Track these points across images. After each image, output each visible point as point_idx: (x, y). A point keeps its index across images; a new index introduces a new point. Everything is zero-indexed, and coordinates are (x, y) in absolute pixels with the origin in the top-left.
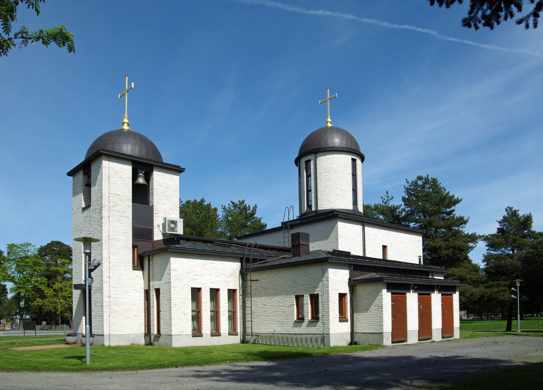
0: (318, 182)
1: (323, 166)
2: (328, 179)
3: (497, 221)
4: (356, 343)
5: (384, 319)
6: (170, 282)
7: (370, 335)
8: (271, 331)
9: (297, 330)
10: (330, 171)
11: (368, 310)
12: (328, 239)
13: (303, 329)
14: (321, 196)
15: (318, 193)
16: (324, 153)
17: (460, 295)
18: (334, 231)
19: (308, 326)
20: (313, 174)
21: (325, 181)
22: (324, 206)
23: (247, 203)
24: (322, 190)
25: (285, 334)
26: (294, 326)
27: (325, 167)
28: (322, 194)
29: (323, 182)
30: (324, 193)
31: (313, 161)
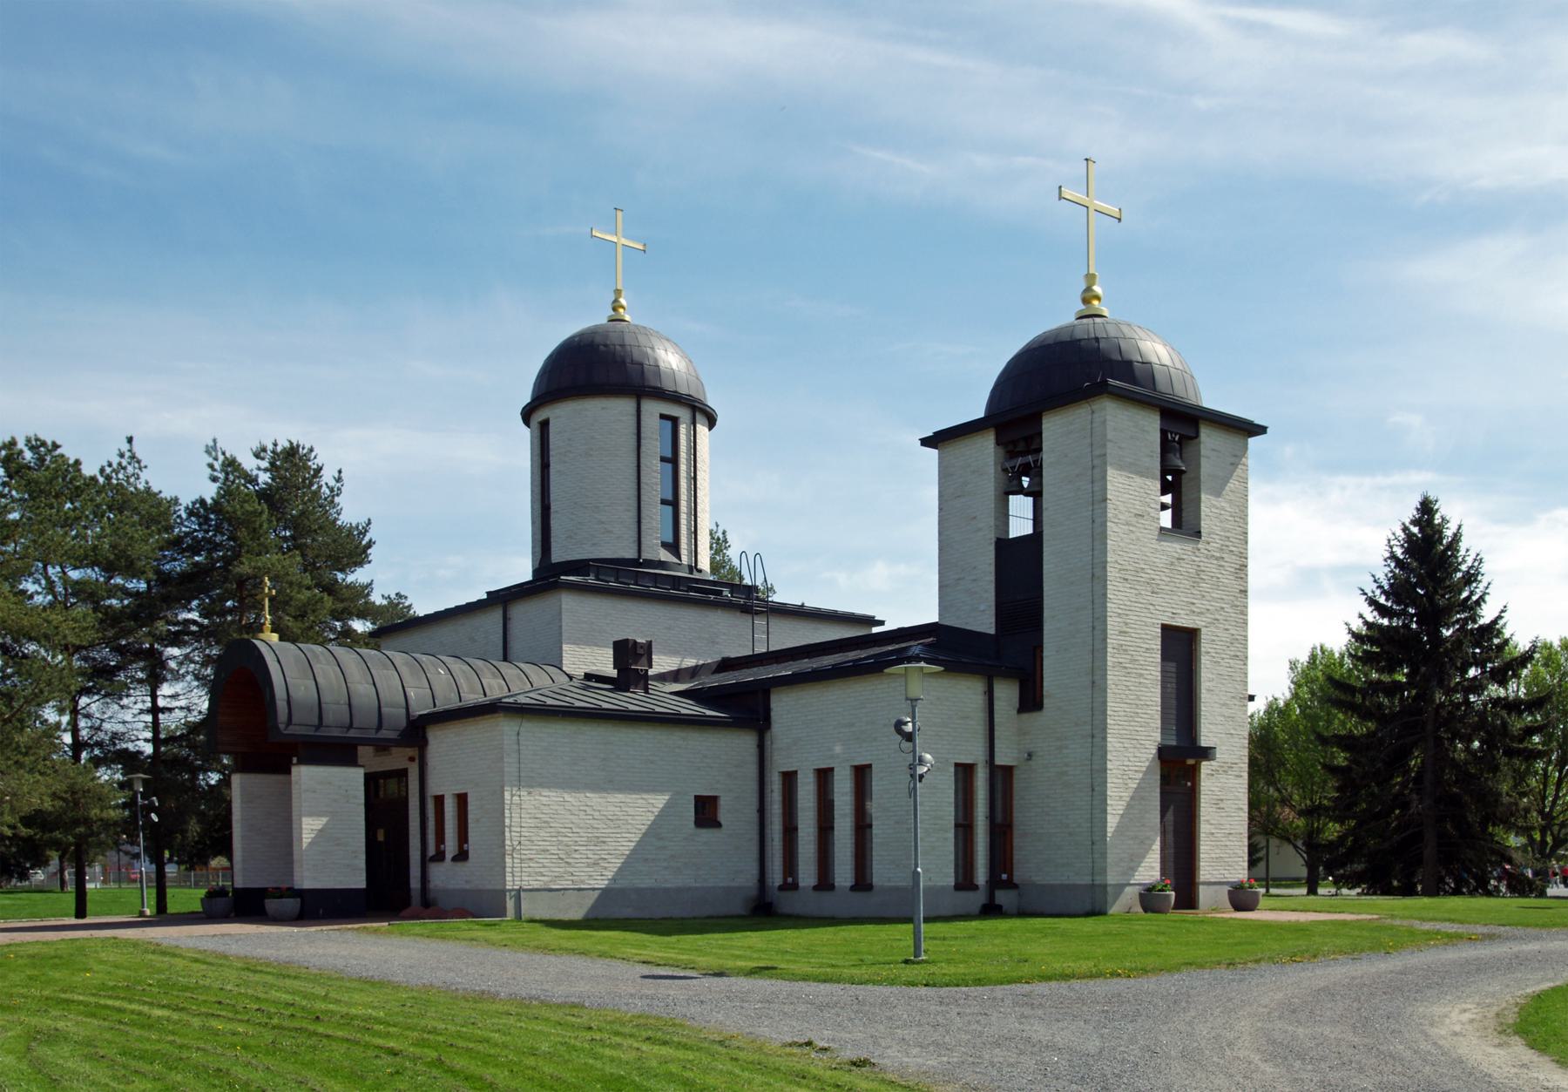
17: (668, 806)
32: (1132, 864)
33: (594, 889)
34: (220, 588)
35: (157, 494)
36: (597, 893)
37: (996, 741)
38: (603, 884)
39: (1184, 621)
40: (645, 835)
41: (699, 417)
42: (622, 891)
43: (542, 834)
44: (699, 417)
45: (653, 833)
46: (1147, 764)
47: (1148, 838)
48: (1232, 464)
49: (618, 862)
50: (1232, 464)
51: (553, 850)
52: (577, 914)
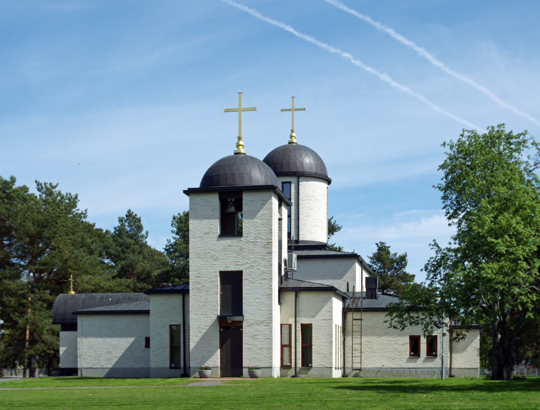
0: (300, 210)
1: (306, 193)
2: (310, 208)
3: (368, 256)
4: (453, 376)
5: (479, 357)
6: (332, 320)
7: (466, 370)
8: (380, 365)
9: (412, 365)
10: (312, 199)
11: (465, 350)
12: (342, 278)
13: (421, 363)
14: (303, 226)
15: (300, 221)
16: (308, 179)
17: (134, 341)
18: (350, 271)
19: (424, 361)
20: (294, 199)
21: (307, 209)
22: (305, 236)
23: (374, 252)
24: (304, 219)
25: (396, 368)
26: (407, 362)
27: (308, 194)
28: (303, 223)
29: (305, 210)
30: (305, 222)
31: (294, 184)
32: (203, 360)
33: (108, 368)
34: (55, 272)
35: (333, 246)
36: (108, 370)
37: (294, 314)
38: (111, 366)
39: (232, 269)
40: (126, 350)
41: (283, 204)
42: (118, 369)
43: (90, 351)
44: (283, 204)
45: (130, 349)
46: (211, 323)
47: (212, 350)
48: (262, 204)
49: (116, 360)
50: (262, 204)
51: (94, 355)
52: (103, 376)
